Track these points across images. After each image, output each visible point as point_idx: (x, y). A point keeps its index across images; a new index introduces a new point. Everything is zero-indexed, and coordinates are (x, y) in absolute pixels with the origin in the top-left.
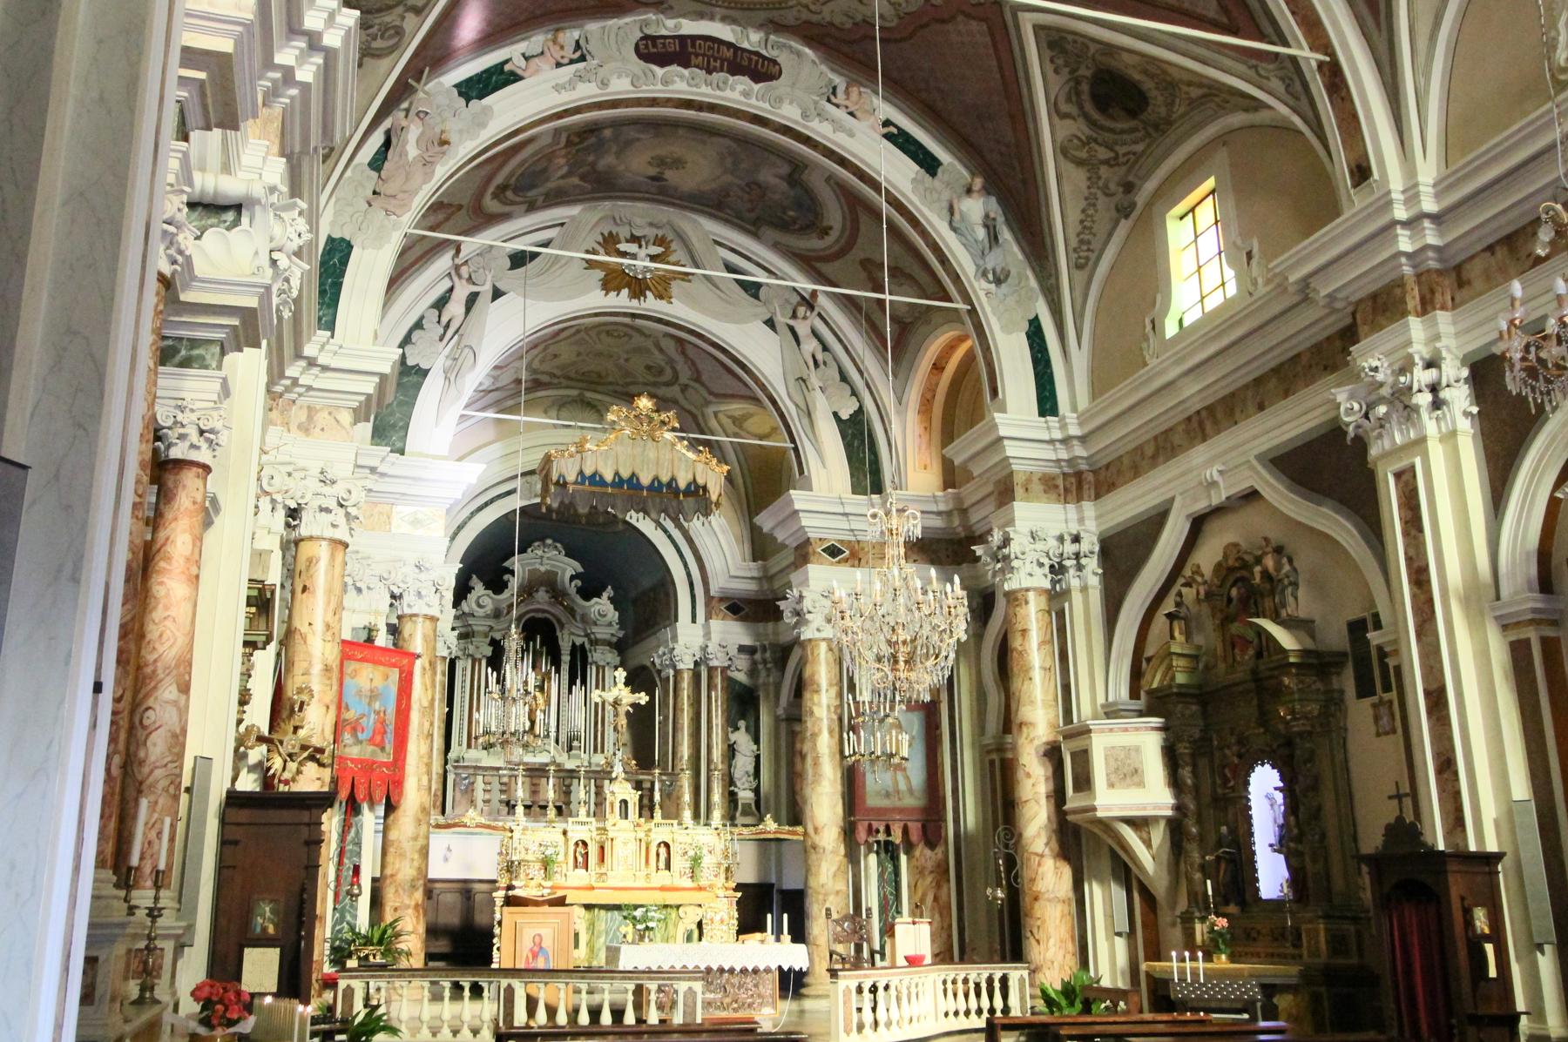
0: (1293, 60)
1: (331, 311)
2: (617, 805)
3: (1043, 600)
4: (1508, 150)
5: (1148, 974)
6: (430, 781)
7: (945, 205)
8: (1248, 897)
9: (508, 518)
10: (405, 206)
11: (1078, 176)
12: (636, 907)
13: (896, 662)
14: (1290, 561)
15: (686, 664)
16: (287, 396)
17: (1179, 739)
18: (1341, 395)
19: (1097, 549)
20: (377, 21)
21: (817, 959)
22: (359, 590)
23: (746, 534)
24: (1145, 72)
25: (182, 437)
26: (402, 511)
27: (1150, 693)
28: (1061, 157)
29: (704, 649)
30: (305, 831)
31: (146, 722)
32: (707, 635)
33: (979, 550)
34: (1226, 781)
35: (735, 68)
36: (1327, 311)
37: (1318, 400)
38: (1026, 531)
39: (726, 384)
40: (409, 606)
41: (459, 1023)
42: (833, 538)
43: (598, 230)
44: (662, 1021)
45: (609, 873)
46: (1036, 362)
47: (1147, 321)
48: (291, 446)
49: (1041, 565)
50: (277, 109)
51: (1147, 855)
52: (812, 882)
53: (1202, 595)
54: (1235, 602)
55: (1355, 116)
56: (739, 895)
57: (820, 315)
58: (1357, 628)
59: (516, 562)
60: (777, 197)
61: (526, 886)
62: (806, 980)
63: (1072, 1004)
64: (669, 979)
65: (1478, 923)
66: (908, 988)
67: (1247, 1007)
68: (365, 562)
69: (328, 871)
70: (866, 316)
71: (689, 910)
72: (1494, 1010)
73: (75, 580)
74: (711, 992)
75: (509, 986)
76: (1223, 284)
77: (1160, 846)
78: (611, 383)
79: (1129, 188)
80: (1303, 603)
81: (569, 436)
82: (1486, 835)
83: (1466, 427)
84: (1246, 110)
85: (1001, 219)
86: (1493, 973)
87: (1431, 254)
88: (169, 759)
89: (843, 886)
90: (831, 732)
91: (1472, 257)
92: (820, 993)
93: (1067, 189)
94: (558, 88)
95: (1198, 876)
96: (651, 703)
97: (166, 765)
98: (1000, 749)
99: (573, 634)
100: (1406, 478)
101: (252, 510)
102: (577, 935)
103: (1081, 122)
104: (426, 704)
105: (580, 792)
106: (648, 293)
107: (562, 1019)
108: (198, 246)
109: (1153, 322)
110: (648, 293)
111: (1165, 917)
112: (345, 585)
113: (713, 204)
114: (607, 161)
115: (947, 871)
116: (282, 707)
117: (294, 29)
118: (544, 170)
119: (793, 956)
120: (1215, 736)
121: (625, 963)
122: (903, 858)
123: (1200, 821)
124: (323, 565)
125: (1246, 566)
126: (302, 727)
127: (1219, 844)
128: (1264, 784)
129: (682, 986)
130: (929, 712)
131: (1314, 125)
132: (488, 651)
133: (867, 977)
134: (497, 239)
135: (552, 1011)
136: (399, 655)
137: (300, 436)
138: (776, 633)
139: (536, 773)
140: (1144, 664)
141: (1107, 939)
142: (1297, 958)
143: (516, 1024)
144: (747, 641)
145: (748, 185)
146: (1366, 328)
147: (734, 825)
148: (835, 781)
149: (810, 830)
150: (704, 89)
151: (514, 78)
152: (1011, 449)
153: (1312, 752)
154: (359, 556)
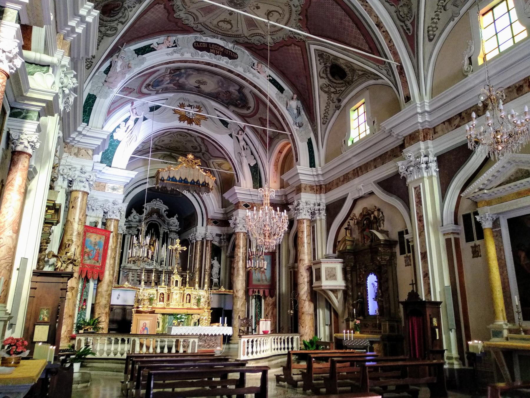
0: (389, 63)
1: (88, 117)
3: (309, 222)
5: (335, 337)
6: (114, 272)
7: (285, 102)
8: (366, 314)
9: (143, 192)
11: (325, 96)
12: (178, 314)
13: (265, 236)
14: (382, 213)
15: (199, 239)
16: (71, 143)
17: (347, 266)
18: (400, 164)
19: (325, 208)
20: (109, 25)
21: (235, 332)
22: (93, 210)
24: (346, 66)
28: (320, 90)
32: (206, 230)
33: (290, 207)
34: (360, 278)
36: (396, 139)
40: (110, 216)
41: (110, 352)
42: (246, 201)
43: (179, 102)
44: (184, 352)
45: (171, 304)
46: (310, 151)
47: (343, 140)
49: (308, 212)
51: (337, 301)
52: (235, 308)
53: (356, 223)
55: (407, 82)
57: (246, 134)
58: (401, 234)
60: (235, 96)
61: (143, 307)
62: (231, 338)
63: (312, 346)
64: (187, 338)
65: (434, 323)
66: (263, 341)
67: (365, 348)
68: (95, 201)
70: (260, 135)
71: (196, 316)
72: (438, 348)
74: (201, 342)
75: (134, 339)
76: (366, 131)
77: (341, 298)
78: (180, 151)
79: (339, 101)
80: (386, 226)
81: (165, 167)
82: (437, 296)
84: (375, 79)
85: (301, 108)
86: (438, 338)
87: (427, 123)
88: (8, 257)
89: (244, 309)
90: (243, 261)
91: (438, 125)
92: (235, 342)
93: (321, 99)
94: (167, 54)
95: (351, 307)
97: (6, 259)
98: (293, 267)
99: (164, 228)
103: (327, 80)
104: (113, 247)
106: (193, 123)
107: (151, 350)
108: (32, 78)
109: (345, 141)
110: (193, 123)
111: (341, 320)
112: (88, 207)
113: (214, 97)
114: (182, 80)
115: (276, 305)
118: (162, 81)
119: (228, 331)
120: (358, 265)
121: (173, 332)
122: (263, 301)
123: (352, 291)
124: (80, 199)
126: (69, 253)
127: (358, 298)
128: (372, 280)
129: (191, 340)
130: (272, 255)
131: (394, 83)
133: (250, 338)
135: (148, 348)
137: (75, 158)
139: (149, 271)
140: (337, 243)
141: (323, 326)
143: (136, 352)
144: (219, 233)
145: (226, 92)
146: (407, 144)
148: (243, 276)
149: (235, 291)
150: (214, 60)
151: (153, 50)
152: (301, 177)
154: (97, 201)
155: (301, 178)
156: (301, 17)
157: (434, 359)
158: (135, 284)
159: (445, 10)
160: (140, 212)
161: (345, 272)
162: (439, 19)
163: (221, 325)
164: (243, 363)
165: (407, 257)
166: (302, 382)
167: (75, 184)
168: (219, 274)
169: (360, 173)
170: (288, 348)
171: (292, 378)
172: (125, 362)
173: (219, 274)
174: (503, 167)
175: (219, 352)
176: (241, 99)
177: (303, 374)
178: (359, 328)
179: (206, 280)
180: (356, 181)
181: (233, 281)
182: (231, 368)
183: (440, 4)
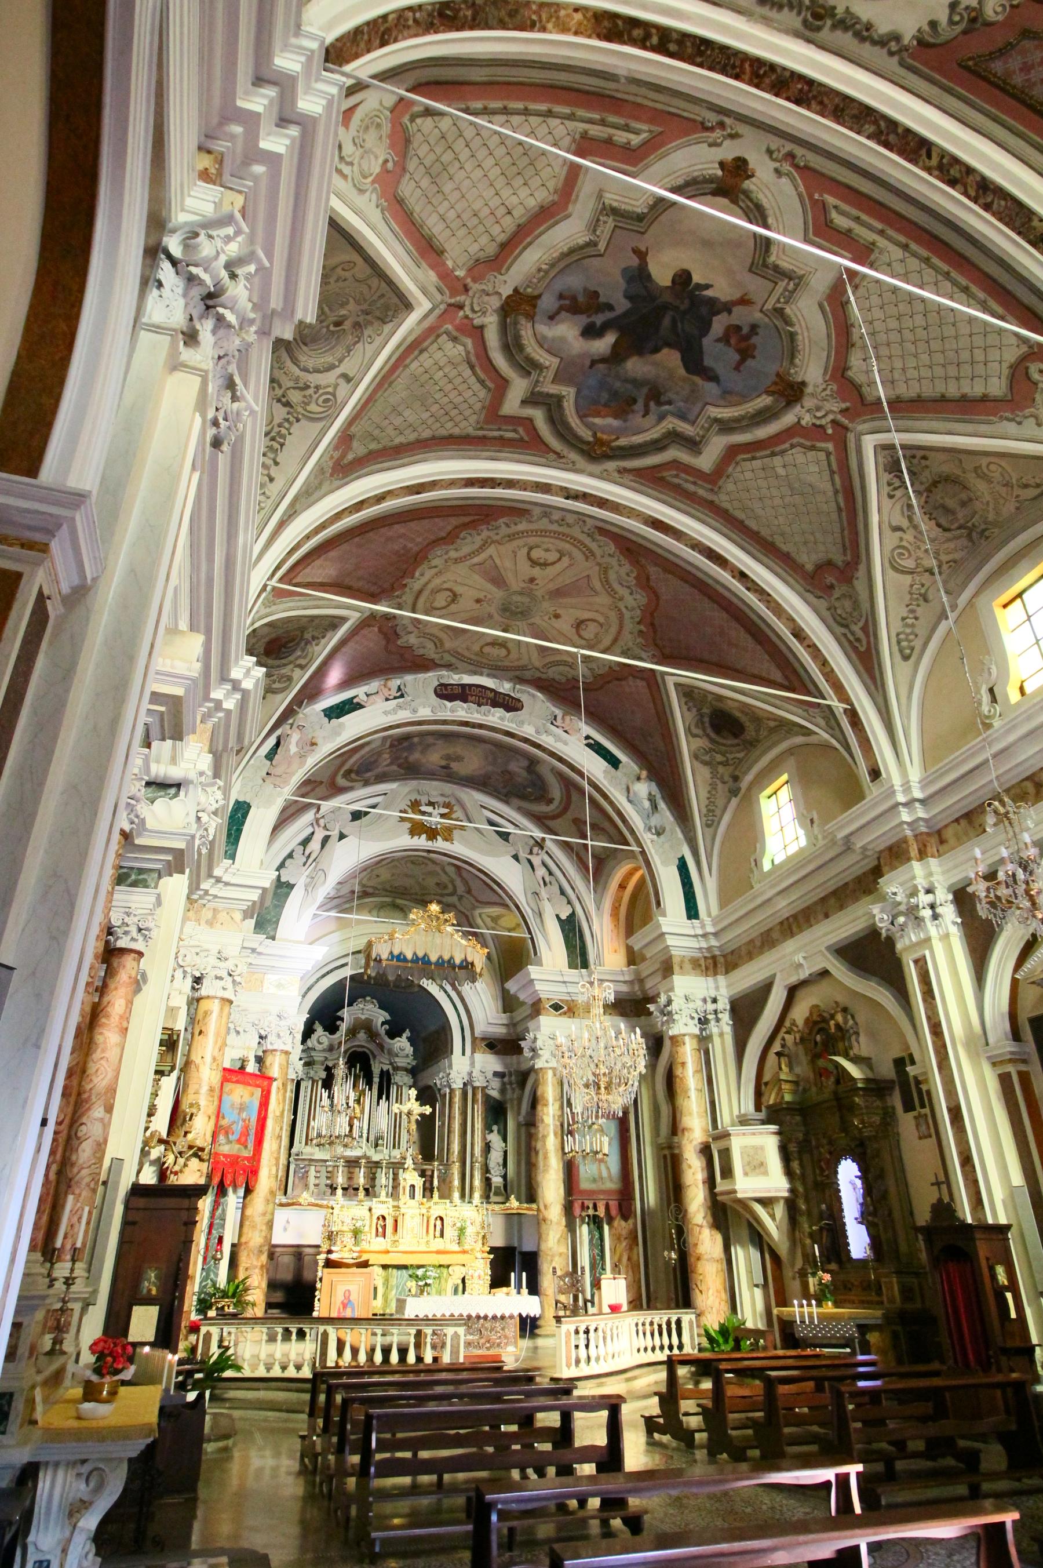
0: (829, 706)
5: (779, 1318)
8: (844, 1259)
9: (341, 983)
10: (286, 782)
11: (705, 772)
13: (599, 1088)
14: (853, 1017)
15: (458, 1085)
17: (790, 1140)
18: (876, 910)
22: (238, 1032)
23: (499, 994)
24: (742, 712)
25: (126, 933)
26: (271, 978)
27: (768, 1107)
29: (470, 1074)
31: (80, 1134)
32: (472, 1064)
33: (652, 1007)
34: (822, 1170)
35: (495, 704)
37: (860, 913)
38: (682, 995)
42: (556, 998)
49: (693, 1018)
50: (209, 725)
52: (543, 1247)
58: (900, 1063)
59: (346, 1013)
63: (726, 1341)
69: (200, 1239)
70: (577, 854)
72: (1018, 1343)
79: (736, 779)
80: (863, 1046)
82: (998, 1213)
85: (658, 796)
86: (1013, 1315)
90: (555, 1134)
94: (386, 713)
95: (808, 1241)
96: (433, 1113)
98: (670, 1147)
100: (921, 963)
102: (375, 1289)
104: (278, 1114)
105: (383, 1179)
107: (362, 1358)
111: (788, 1273)
112: (229, 1029)
114: (415, 756)
117: (224, 678)
118: (376, 761)
119: (528, 1305)
121: (409, 1313)
122: (606, 1228)
123: (807, 1200)
124: (214, 1016)
125: (825, 1020)
127: (821, 1218)
128: (848, 1172)
129: (450, 1331)
132: (323, 1075)
133: (582, 1322)
135: (355, 1351)
136: (263, 1079)
138: (519, 1063)
139: (352, 1164)
144: (499, 1068)
147: (488, 1203)
149: (542, 1207)
150: (476, 715)
151: (360, 706)
152: (670, 941)
155: (669, 942)
156: (642, 628)
157: (1012, 1370)
158: (321, 1195)
159: (926, 600)
160: (332, 1028)
161: (784, 1151)
162: (916, 618)
164: (563, 1388)
165: (920, 1115)
166: (705, 1435)
168: (505, 1164)
169: (795, 929)
170: (671, 1348)
171: (681, 1422)
172: (309, 1386)
173: (505, 1164)
175: (513, 1359)
176: (533, 784)
177: (705, 1412)
178: (831, 1293)
181: (537, 1182)
182: (543, 1401)
183: (914, 590)
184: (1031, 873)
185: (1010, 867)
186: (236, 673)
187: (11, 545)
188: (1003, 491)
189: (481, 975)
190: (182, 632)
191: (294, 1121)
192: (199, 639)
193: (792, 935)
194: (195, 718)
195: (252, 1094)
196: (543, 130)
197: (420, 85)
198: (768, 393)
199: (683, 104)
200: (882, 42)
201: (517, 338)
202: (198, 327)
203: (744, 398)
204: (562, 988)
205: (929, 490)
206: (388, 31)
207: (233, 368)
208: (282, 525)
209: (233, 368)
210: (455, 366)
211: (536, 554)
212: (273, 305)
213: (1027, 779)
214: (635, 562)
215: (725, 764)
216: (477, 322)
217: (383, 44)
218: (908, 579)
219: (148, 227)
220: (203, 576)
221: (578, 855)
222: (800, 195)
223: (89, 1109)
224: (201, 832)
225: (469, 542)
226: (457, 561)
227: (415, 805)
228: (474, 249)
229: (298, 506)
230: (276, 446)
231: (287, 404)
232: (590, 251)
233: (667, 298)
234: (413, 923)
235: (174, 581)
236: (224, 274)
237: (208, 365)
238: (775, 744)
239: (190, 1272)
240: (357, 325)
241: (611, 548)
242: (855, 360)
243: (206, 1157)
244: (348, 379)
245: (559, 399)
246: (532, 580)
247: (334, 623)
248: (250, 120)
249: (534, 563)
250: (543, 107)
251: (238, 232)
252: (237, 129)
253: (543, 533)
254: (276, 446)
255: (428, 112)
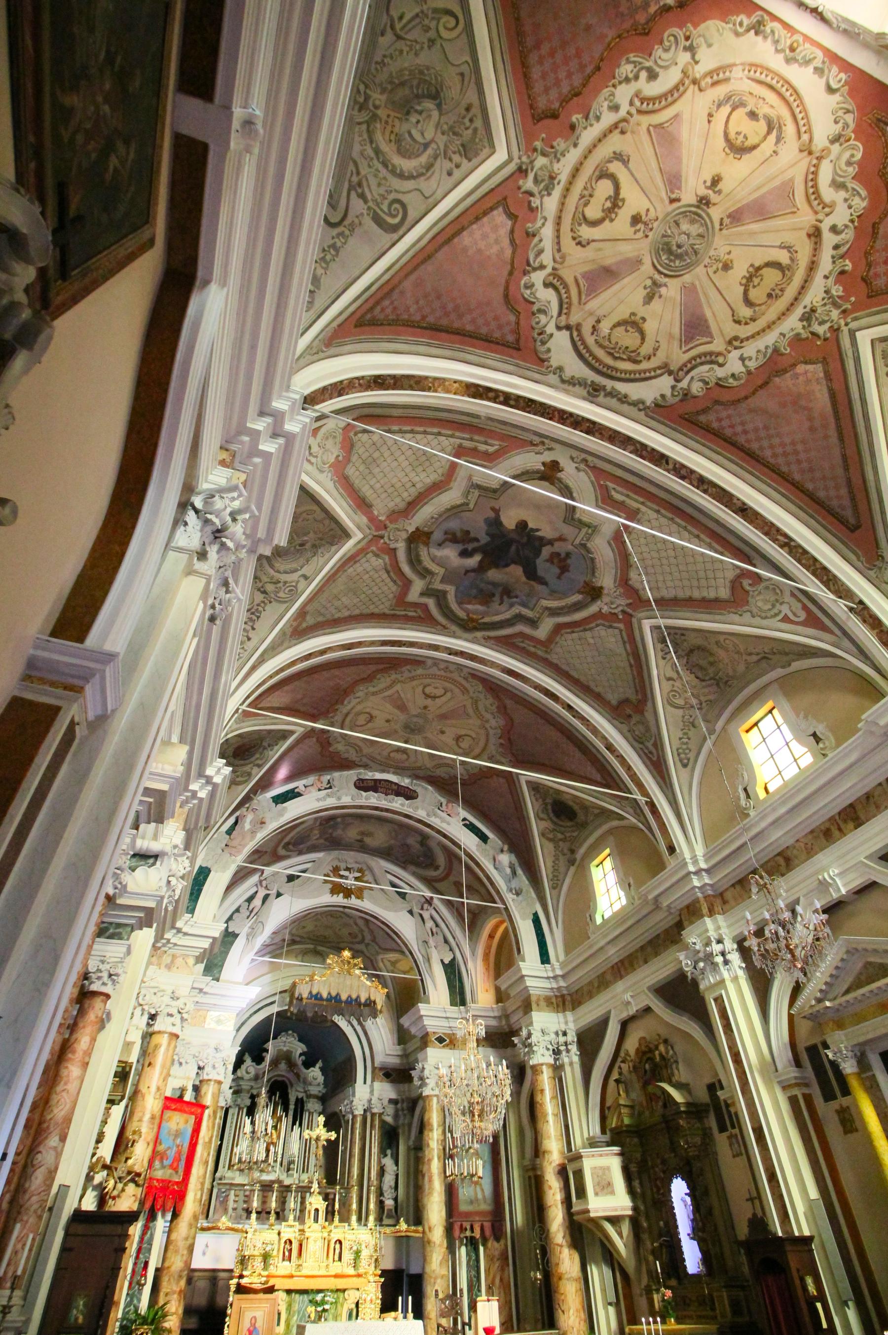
0: (635, 800)
2: (313, 1213)
3: (550, 1070)
4: (732, 841)
9: (268, 1019)
10: (240, 852)
11: (550, 846)
13: (473, 1116)
15: (359, 1111)
18: (682, 956)
22: (181, 1064)
23: (395, 1029)
25: (99, 978)
26: (213, 1014)
27: (612, 1130)
29: (370, 1101)
30: (116, 1240)
31: (35, 1162)
32: (372, 1092)
33: (515, 1040)
35: (398, 794)
37: (670, 958)
38: (539, 1029)
39: (390, 944)
42: (441, 1032)
48: (161, 978)
50: (186, 809)
52: (428, 1270)
54: (648, 1073)
56: (382, 1280)
58: (713, 1088)
59: (270, 1045)
69: (128, 1264)
70: (456, 909)
73: (9, 1086)
79: (572, 851)
80: (682, 1074)
81: (307, 971)
82: (803, 1227)
83: (741, 974)
86: (825, 1326)
89: (446, 1271)
90: (439, 1158)
93: (545, 850)
94: (318, 800)
95: (651, 1258)
96: (338, 1137)
100: (719, 1000)
101: (129, 1015)
102: (279, 1314)
104: (207, 1140)
105: (292, 1203)
111: (636, 1290)
112: (173, 1060)
113: (386, 853)
115: (507, 1258)
116: (122, 1144)
117: (201, 774)
122: (481, 1249)
123: (648, 1218)
124: (162, 1050)
125: (651, 1051)
128: (679, 1189)
132: (248, 1102)
134: (281, 869)
136: (197, 1108)
138: (409, 1091)
139: (267, 1187)
142: (714, 1318)
144: (393, 1096)
147: (381, 1225)
149: (427, 1230)
151: (299, 795)
152: (529, 982)
153: (702, 1170)
156: (502, 741)
159: (694, 726)
161: (626, 1171)
163: (401, 1316)
167: (159, 1019)
168: (396, 1187)
174: (842, 960)
179: (372, 1206)
180: (620, 986)
184: (788, 932)
185: (772, 927)
186: (210, 771)
187: (57, 687)
188: (736, 656)
189: (381, 1012)
190: (173, 744)
191: (220, 1146)
192: (186, 748)
193: (621, 977)
194: (175, 803)
195: (186, 1122)
196: (435, 442)
197: (361, 417)
198: (579, 592)
199: (520, 432)
200: (634, 404)
201: (418, 556)
202: (208, 549)
203: (564, 595)
204: (445, 1023)
205: (688, 655)
206: (343, 389)
207: (229, 573)
208: (254, 668)
209: (229, 573)
210: (377, 571)
211: (428, 690)
212: (259, 535)
213: (779, 854)
214: (497, 697)
215: (564, 840)
216: (392, 546)
217: (340, 395)
218: (680, 712)
219: (182, 491)
220: (194, 703)
221: (457, 910)
222: (592, 483)
223: (46, 1138)
224: (170, 893)
225: (383, 681)
226: (374, 694)
227: (336, 871)
228: (391, 505)
229: (266, 656)
230: (254, 618)
231: (265, 592)
232: (464, 508)
233: (514, 536)
234: (329, 967)
235: (172, 707)
236: (229, 519)
237: (212, 572)
238: (600, 825)
239: (116, 1298)
240: (314, 546)
241: (481, 688)
242: (633, 575)
243: (141, 1182)
244: (305, 577)
245: (444, 593)
246: (425, 707)
247: (284, 735)
248: (255, 435)
249: (427, 696)
250: (435, 430)
251: (239, 496)
252: (246, 439)
253: (434, 677)
254: (254, 618)
255: (365, 431)
